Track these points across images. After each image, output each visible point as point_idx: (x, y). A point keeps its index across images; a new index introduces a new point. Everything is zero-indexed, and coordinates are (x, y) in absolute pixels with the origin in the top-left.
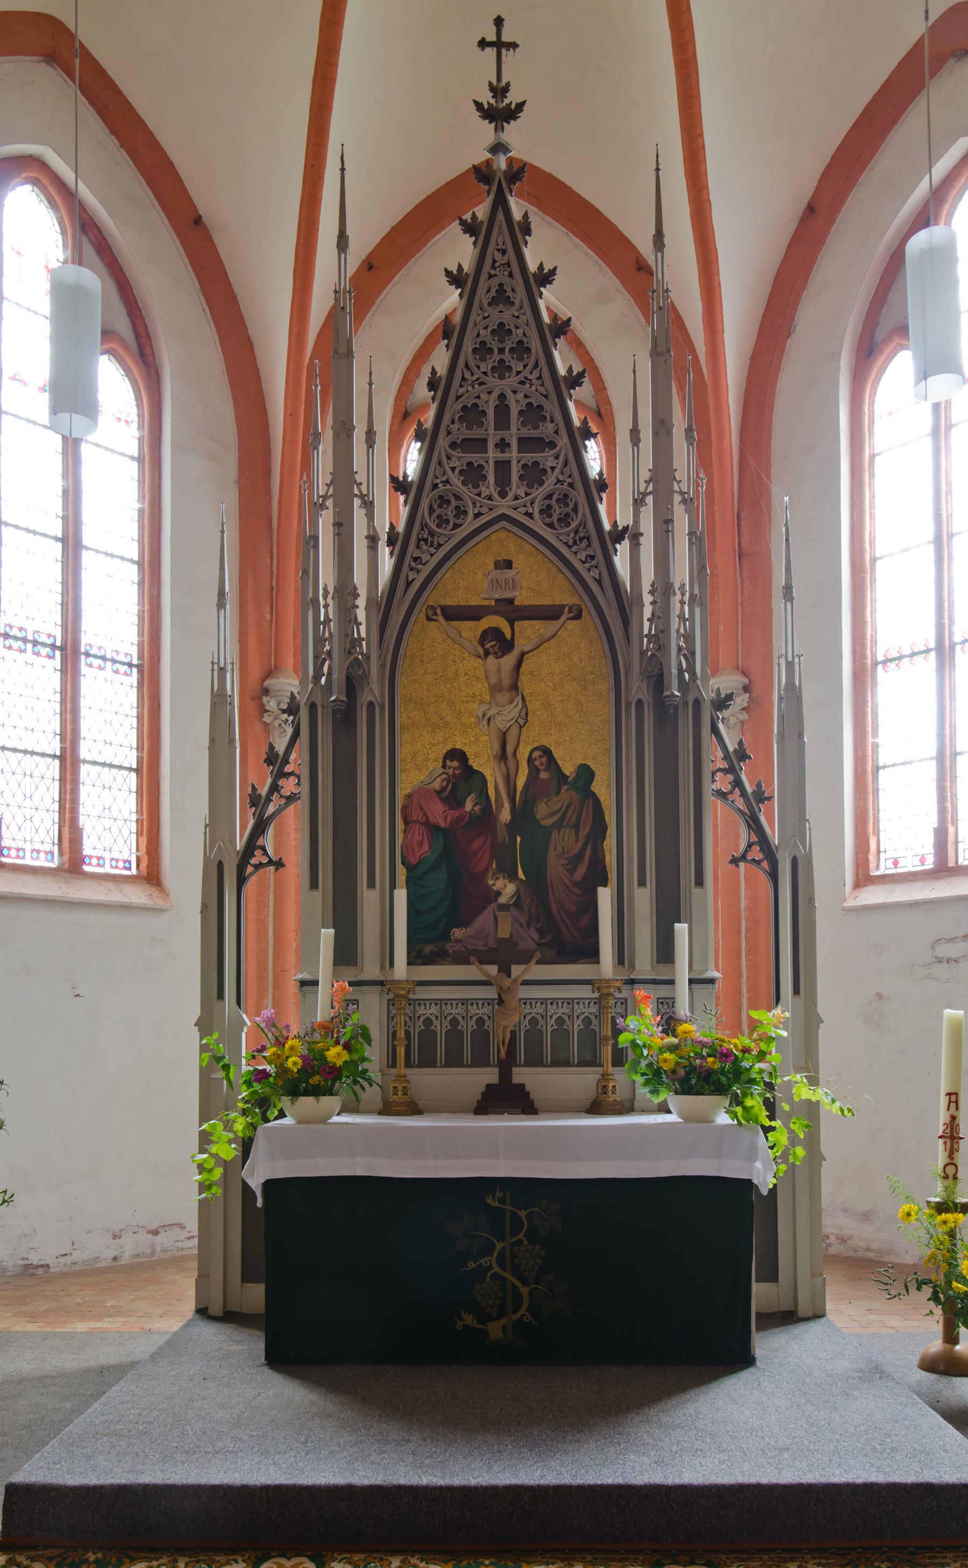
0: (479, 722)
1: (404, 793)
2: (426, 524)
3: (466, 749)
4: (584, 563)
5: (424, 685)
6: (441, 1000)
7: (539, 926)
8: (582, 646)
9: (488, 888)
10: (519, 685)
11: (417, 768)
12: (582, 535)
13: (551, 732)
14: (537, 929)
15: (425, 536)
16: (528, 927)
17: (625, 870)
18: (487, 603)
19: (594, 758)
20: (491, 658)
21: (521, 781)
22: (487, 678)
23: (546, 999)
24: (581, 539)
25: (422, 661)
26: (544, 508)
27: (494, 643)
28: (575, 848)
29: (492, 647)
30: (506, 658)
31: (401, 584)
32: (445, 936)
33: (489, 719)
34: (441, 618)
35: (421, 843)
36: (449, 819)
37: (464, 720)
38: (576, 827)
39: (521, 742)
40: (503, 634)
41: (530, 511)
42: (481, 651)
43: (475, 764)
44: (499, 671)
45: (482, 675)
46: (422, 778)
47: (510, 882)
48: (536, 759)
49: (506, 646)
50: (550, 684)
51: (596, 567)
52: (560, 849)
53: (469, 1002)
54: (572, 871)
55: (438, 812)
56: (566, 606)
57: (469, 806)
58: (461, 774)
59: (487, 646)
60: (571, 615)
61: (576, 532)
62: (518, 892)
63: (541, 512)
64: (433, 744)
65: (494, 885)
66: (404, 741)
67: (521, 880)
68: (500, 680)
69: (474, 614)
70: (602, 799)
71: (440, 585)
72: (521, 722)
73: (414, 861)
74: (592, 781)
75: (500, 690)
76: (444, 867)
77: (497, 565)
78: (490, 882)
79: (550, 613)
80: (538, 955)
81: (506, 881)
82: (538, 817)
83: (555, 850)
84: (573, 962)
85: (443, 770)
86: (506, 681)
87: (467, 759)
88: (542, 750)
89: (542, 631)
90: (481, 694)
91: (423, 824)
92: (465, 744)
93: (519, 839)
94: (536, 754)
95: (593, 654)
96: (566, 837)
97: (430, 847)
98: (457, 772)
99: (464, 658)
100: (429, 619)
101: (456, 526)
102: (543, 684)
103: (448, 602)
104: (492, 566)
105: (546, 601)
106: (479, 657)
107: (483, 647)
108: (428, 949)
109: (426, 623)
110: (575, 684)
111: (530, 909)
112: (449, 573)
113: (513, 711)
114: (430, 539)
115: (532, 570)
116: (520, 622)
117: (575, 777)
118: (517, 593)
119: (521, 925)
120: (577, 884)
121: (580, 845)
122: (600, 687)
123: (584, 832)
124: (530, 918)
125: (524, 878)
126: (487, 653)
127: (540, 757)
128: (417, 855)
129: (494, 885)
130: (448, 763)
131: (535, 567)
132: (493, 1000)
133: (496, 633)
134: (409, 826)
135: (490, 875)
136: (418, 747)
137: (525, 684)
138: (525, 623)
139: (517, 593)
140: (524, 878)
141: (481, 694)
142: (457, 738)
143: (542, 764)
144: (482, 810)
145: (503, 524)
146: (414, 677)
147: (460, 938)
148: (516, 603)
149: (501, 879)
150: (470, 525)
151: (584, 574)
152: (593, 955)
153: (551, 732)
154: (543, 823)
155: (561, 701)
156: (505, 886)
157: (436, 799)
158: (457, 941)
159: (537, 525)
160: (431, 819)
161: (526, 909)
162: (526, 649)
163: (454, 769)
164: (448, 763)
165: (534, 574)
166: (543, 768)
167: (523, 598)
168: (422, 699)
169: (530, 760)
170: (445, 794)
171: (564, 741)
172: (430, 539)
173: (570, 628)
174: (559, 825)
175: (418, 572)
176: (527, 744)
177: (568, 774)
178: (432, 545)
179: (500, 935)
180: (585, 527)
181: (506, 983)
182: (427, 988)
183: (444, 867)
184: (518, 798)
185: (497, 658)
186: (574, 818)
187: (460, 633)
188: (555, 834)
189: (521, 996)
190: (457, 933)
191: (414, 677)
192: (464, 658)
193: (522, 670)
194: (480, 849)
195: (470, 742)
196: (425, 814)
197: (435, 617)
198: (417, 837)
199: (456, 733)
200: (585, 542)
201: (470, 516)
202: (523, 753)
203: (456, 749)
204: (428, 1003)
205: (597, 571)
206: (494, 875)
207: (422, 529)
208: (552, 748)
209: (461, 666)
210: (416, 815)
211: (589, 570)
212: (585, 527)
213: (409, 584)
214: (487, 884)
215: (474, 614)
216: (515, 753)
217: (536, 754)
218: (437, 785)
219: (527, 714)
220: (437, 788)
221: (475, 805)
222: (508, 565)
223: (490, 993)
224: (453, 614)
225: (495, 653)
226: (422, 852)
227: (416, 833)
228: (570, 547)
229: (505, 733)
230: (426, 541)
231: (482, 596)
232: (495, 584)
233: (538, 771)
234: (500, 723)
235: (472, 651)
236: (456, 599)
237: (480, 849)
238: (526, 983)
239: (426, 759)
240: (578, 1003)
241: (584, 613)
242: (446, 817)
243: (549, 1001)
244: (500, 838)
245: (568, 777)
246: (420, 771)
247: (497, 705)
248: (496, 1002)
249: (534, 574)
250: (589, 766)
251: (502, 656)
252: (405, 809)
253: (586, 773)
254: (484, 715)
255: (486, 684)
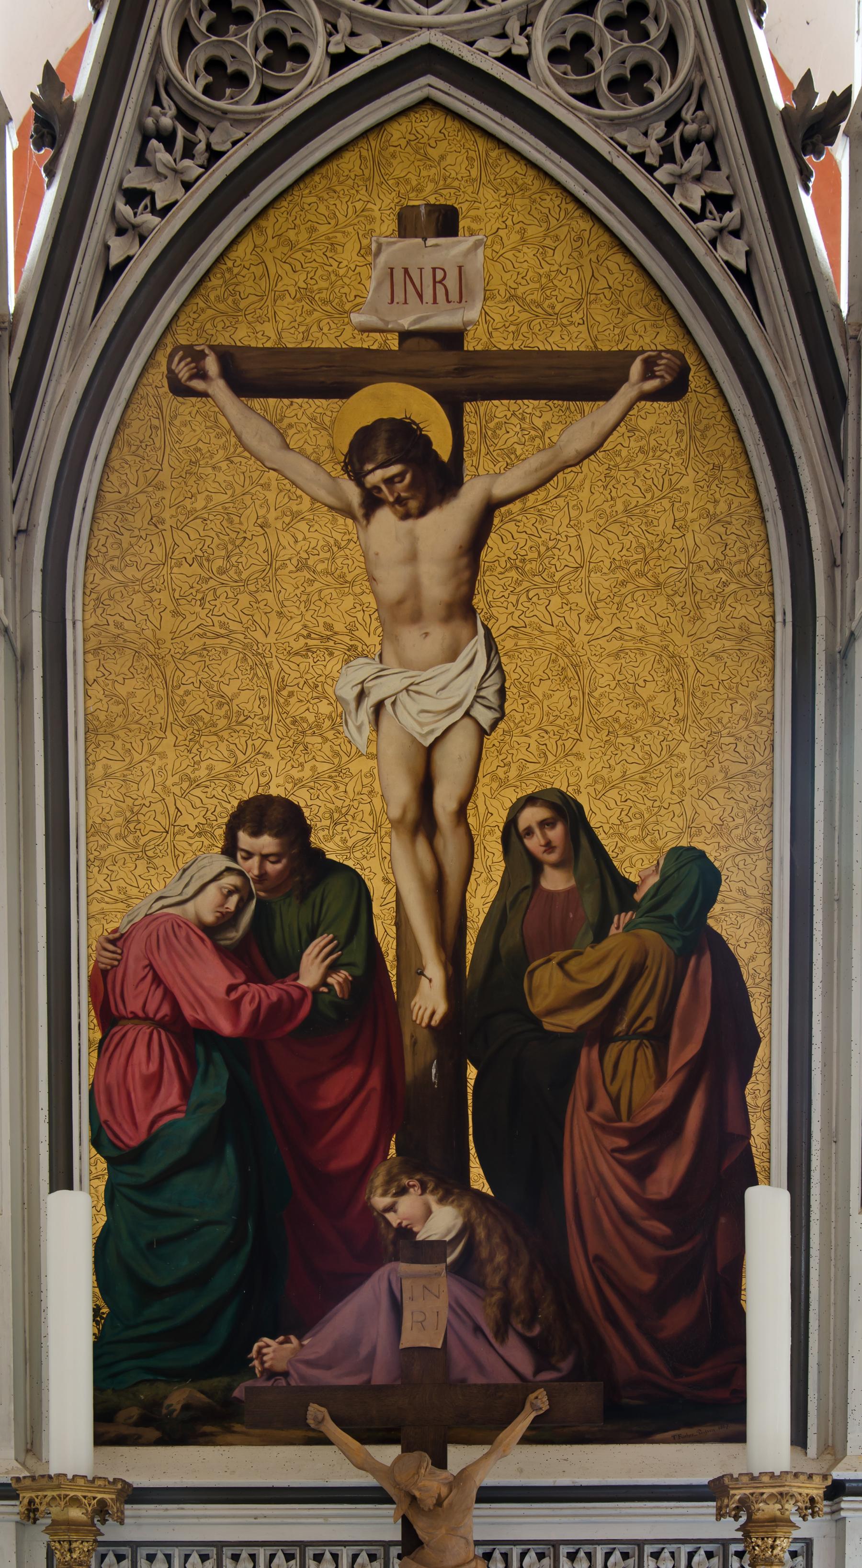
0: (344, 718)
1: (97, 930)
2: (169, 83)
3: (301, 798)
4: (696, 217)
5: (164, 597)
6: (220, 1545)
7: (537, 1330)
8: (686, 482)
9: (373, 1220)
10: (478, 602)
11: (142, 853)
12: (691, 129)
13: (583, 747)
14: (529, 1343)
15: (167, 121)
16: (501, 1332)
17: (816, 1162)
18: (372, 342)
19: (720, 828)
20: (385, 517)
21: (480, 900)
22: (372, 579)
23: (555, 1545)
24: (687, 147)
25: (155, 522)
26: (565, 43)
27: (395, 469)
28: (652, 1099)
29: (389, 481)
30: (435, 517)
31: (85, 271)
32: (234, 1359)
33: (379, 707)
34: (219, 388)
35: (154, 1082)
36: (247, 1009)
37: (295, 708)
38: (659, 1038)
39: (482, 780)
40: (428, 442)
41: (520, 49)
42: (353, 494)
43: (330, 844)
44: (412, 557)
45: (356, 570)
46: (159, 886)
47: (442, 1201)
48: (529, 832)
49: (437, 480)
50: (580, 599)
51: (736, 234)
52: (604, 1104)
53: (310, 1552)
54: (642, 1171)
55: (210, 988)
56: (633, 355)
57: (310, 972)
58: (293, 876)
59: (375, 478)
60: (651, 385)
61: (674, 122)
62: (467, 1229)
63: (556, 56)
64: (195, 783)
65: (391, 1208)
66: (98, 772)
67: (478, 1194)
68: (415, 587)
69: (328, 376)
70: (742, 954)
71: (215, 281)
72: (485, 717)
73: (132, 1138)
74: (710, 899)
75: (416, 617)
76: (229, 1153)
77: (408, 224)
78: (380, 1202)
79: (583, 380)
80: (540, 1401)
81: (431, 1199)
82: (537, 1006)
83: (590, 1106)
84: (739, 1317)
85: (225, 862)
86: (436, 587)
87: (306, 830)
88: (551, 805)
89: (553, 433)
90: (351, 631)
91: (161, 1024)
92: (298, 783)
93: (472, 1073)
94: (531, 816)
95: (722, 507)
96: (625, 1065)
97: (185, 1093)
98: (272, 868)
99: (296, 516)
100: (179, 389)
101: (267, 94)
102: (556, 601)
103: (241, 336)
104: (390, 225)
105: (571, 340)
106: (348, 512)
107: (360, 483)
108: (178, 1397)
109: (170, 402)
110: (661, 602)
111: (505, 1282)
112: (243, 249)
113: (458, 682)
114: (181, 132)
115: (523, 241)
116: (484, 406)
117: (658, 887)
118: (473, 313)
119: (477, 1329)
120: (656, 1209)
121: (669, 1091)
122: (742, 610)
123: (684, 1052)
124: (506, 1308)
125: (487, 1189)
126: (372, 502)
127: (543, 824)
128: (144, 1121)
129: (391, 1208)
130: (244, 839)
131: (533, 231)
132: (387, 1545)
133: (404, 439)
134: (117, 1031)
135: (379, 1178)
136: (146, 788)
137: (494, 592)
138: (500, 408)
139: (473, 313)
140: (487, 1189)
141: (351, 631)
142: (272, 763)
143: (549, 846)
144: (355, 986)
145: (427, 107)
146: (130, 572)
147: (281, 1366)
148: (470, 345)
149: (415, 1192)
150: (313, 84)
151: (699, 248)
152: (721, 1411)
153: (583, 747)
154: (550, 1024)
155: (617, 655)
156: (429, 1212)
157: (207, 951)
158: (271, 1374)
159: (544, 87)
160: (188, 1012)
161: (494, 1280)
162: (501, 490)
163: (264, 857)
164: (244, 839)
165: (529, 252)
166: (553, 857)
167: (489, 327)
168: (158, 643)
169: (511, 834)
170: (235, 935)
171: (624, 777)
172: (181, 132)
173: (646, 425)
174: (601, 1032)
175: (142, 239)
176: (504, 784)
177: (634, 878)
178: (188, 152)
179: (410, 1338)
180: (699, 107)
181: (431, 1484)
182: (173, 1509)
183: (229, 1153)
184: (470, 948)
185: (406, 516)
186: (651, 1011)
187: (282, 436)
188: (588, 1058)
189: (479, 1534)
190: (272, 1351)
191: (130, 572)
192: (296, 516)
193: (487, 556)
194: (345, 1105)
195: (316, 778)
196: (169, 995)
197: (198, 384)
198: (142, 1064)
199: (270, 748)
200: (699, 156)
201: (317, 59)
202: (490, 813)
203: (269, 799)
204: (177, 1554)
205: (739, 246)
206: (388, 1183)
207: (157, 101)
208: (582, 799)
209: (286, 539)
210: (138, 997)
211: (713, 242)
212: (699, 107)
213: (112, 275)
214: (368, 1208)
215: (328, 376)
216: (461, 814)
217: (531, 816)
218: (206, 907)
219: (502, 693)
220: (209, 917)
221: (332, 968)
222: (446, 222)
223: (381, 1525)
224: (259, 376)
225: (399, 501)
226: (156, 1110)
227: (141, 1052)
228: (651, 170)
229: (429, 751)
230: (168, 140)
231: (356, 318)
232: (402, 282)
233: (537, 866)
234: (416, 719)
235: (322, 494)
236: (269, 329)
237: (345, 1105)
238: (490, 1495)
239: (172, 829)
240: (656, 1555)
241: (696, 379)
242: (237, 1003)
243: (564, 1550)
244: (410, 1070)
245: (633, 887)
246: (150, 863)
247: (405, 664)
248: (395, 1551)
249: (529, 252)
250: (702, 855)
251: (423, 512)
252: (102, 981)
253: (693, 878)
254: (361, 696)
255: (369, 598)
